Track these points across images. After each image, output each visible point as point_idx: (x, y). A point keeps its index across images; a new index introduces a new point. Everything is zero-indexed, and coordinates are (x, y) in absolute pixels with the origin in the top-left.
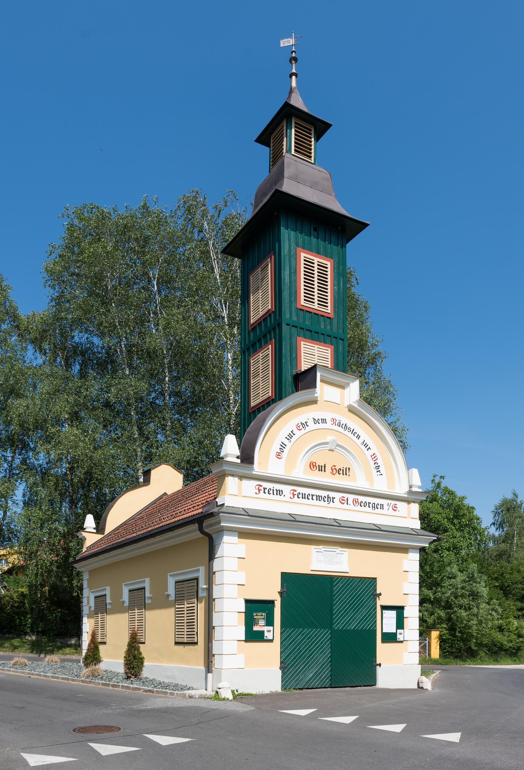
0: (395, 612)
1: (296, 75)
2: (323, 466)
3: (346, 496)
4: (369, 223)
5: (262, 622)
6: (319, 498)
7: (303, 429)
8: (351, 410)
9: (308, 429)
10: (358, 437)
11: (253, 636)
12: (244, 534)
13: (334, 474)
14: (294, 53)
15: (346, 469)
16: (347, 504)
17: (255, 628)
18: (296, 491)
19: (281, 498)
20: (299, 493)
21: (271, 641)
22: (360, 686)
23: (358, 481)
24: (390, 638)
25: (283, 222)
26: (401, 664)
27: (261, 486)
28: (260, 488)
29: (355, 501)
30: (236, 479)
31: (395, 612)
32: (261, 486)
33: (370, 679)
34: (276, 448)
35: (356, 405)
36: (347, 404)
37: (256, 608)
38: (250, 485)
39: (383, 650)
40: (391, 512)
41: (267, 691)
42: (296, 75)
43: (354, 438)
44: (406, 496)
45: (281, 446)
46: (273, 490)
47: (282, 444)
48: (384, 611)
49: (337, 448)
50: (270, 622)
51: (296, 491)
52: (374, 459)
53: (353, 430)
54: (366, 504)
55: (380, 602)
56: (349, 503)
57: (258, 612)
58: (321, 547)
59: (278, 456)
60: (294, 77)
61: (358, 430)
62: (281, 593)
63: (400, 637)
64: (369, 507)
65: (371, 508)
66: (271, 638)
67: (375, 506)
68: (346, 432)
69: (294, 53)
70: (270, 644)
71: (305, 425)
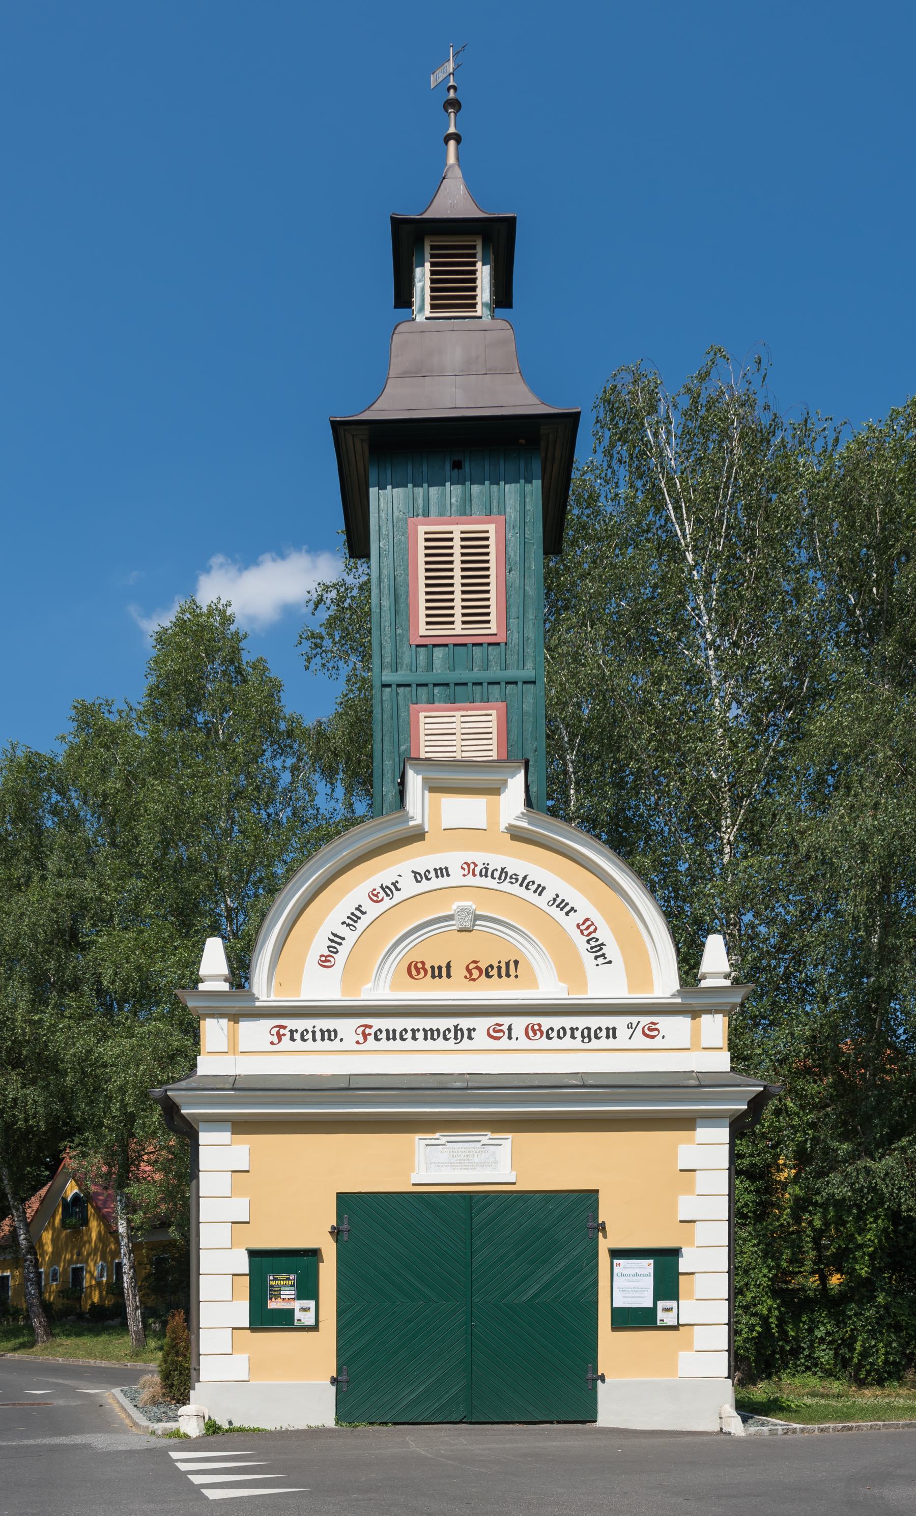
0: (652, 1261)
1: (457, 138)
2: (444, 965)
3: (506, 1021)
4: (579, 410)
5: (288, 1293)
6: (430, 1034)
7: (386, 899)
8: (516, 835)
9: (398, 896)
10: (540, 890)
11: (265, 1319)
12: (241, 1126)
13: (474, 980)
14: (452, 91)
15: (508, 964)
16: (510, 1038)
17: (272, 1305)
18: (370, 1027)
19: (336, 1045)
20: (380, 1031)
21: (315, 1328)
22: (551, 1423)
23: (549, 988)
24: (632, 1319)
25: (373, 476)
26: (671, 1378)
27: (284, 1027)
28: (282, 1031)
29: (532, 1031)
30: (224, 1022)
31: (652, 1261)
32: (284, 1027)
33: (585, 1412)
34: (320, 946)
35: (524, 824)
36: (503, 826)
37: (266, 1264)
38: (254, 1032)
39: (612, 1345)
40: (640, 1040)
41: (302, 1426)
42: (457, 138)
43: (530, 895)
44: (679, 1000)
45: (332, 941)
46: (314, 1032)
47: (332, 937)
48: (615, 1261)
49: (478, 922)
50: (308, 1289)
51: (370, 1027)
52: (586, 933)
53: (525, 878)
54: (562, 1033)
55: (604, 1245)
56: (514, 1036)
57: (280, 1272)
58: (437, 1135)
59: (325, 962)
60: (452, 143)
61: (538, 874)
62: (336, 1232)
63: (663, 1317)
64: (573, 1037)
65: (579, 1038)
66: (311, 1322)
67: (588, 1035)
68: (506, 886)
69: (452, 91)
70: (312, 1334)
71: (390, 890)
